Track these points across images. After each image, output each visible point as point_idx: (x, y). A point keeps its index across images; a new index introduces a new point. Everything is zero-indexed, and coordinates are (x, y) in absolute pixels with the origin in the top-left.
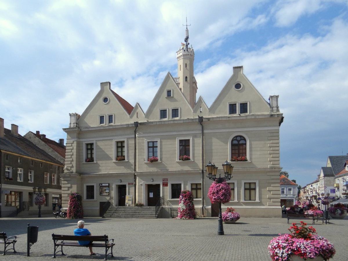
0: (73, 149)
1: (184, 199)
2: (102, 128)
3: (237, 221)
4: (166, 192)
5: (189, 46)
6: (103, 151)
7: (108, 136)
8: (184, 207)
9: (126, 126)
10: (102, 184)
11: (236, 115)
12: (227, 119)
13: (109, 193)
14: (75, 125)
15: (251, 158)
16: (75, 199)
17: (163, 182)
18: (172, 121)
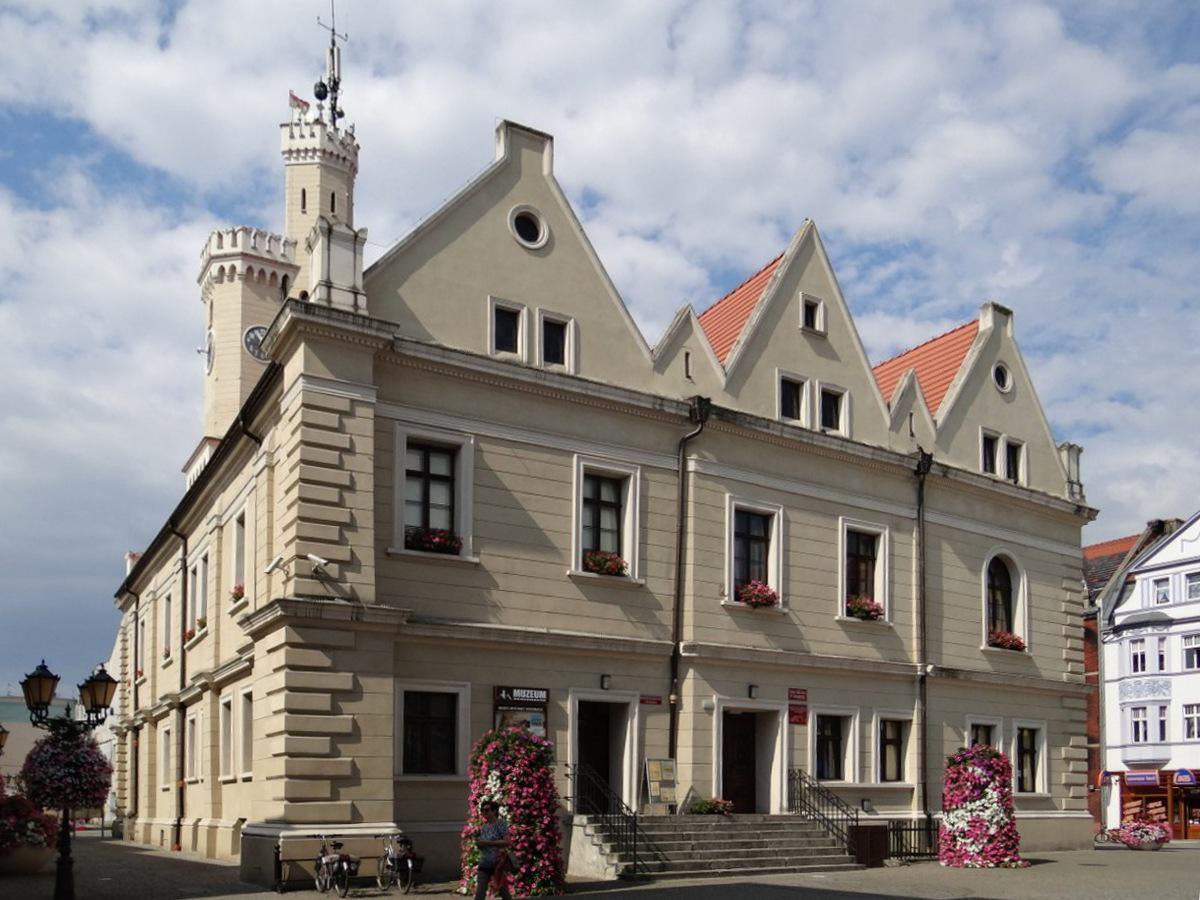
0: (350, 451)
6: (517, 506)
7: (547, 433)
9: (650, 406)
10: (510, 690)
17: (790, 705)
18: (836, 441)
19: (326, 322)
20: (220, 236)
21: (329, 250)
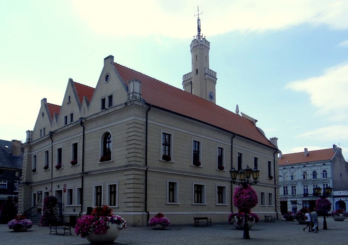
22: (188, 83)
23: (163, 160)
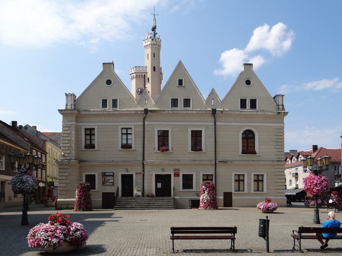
1: (208, 190)
2: (106, 113)
3: (274, 211)
4: (176, 183)
5: (157, 36)
8: (209, 198)
9: (134, 113)
11: (246, 110)
12: (239, 113)
13: (113, 182)
14: (73, 106)
15: (172, 149)
16: (84, 189)
17: (174, 173)
19: (64, 112)
20: (131, 69)
21: (67, 98)
22: (133, 77)
23: (122, 149)
